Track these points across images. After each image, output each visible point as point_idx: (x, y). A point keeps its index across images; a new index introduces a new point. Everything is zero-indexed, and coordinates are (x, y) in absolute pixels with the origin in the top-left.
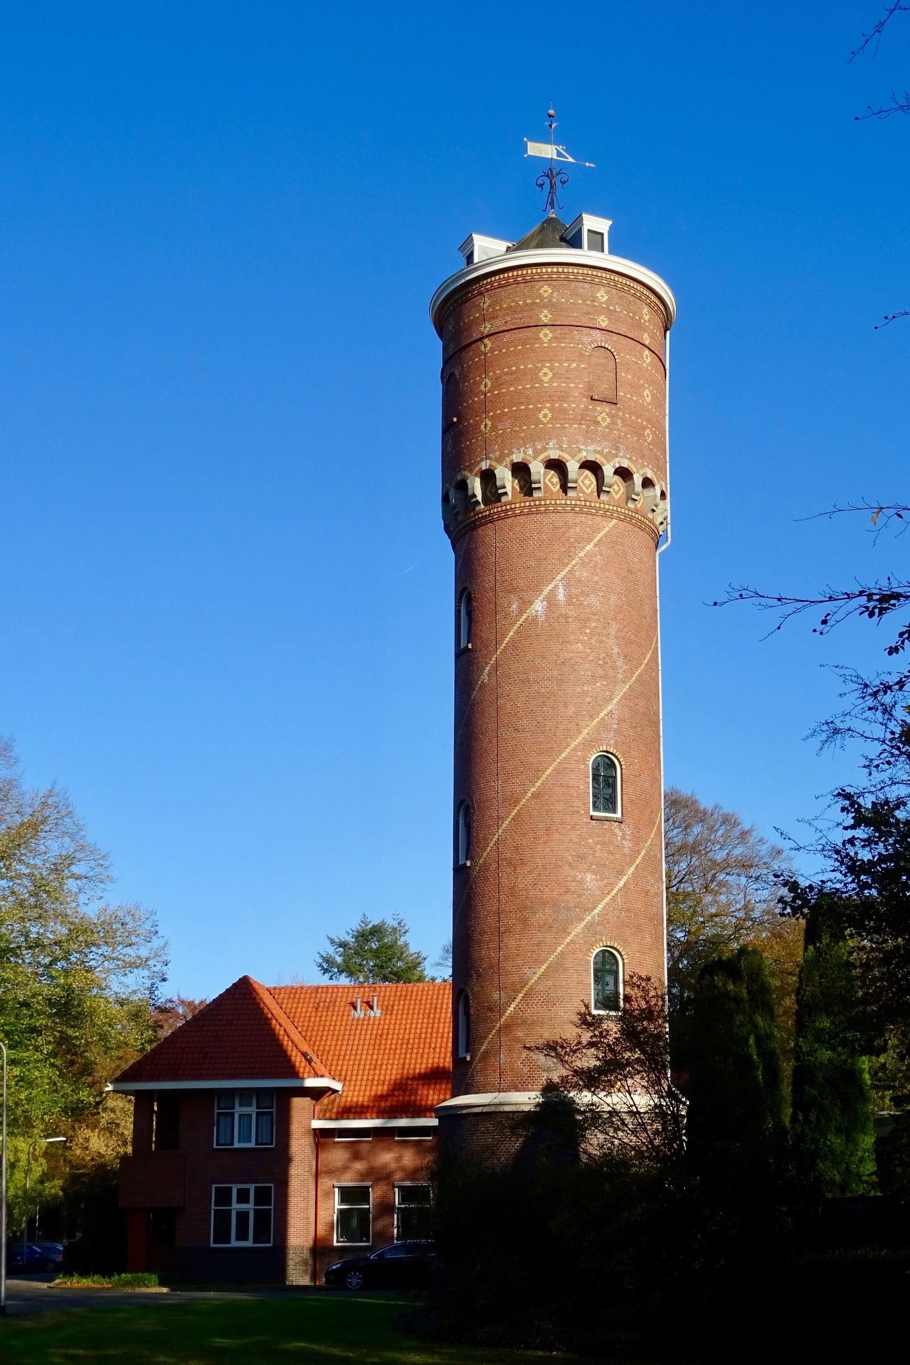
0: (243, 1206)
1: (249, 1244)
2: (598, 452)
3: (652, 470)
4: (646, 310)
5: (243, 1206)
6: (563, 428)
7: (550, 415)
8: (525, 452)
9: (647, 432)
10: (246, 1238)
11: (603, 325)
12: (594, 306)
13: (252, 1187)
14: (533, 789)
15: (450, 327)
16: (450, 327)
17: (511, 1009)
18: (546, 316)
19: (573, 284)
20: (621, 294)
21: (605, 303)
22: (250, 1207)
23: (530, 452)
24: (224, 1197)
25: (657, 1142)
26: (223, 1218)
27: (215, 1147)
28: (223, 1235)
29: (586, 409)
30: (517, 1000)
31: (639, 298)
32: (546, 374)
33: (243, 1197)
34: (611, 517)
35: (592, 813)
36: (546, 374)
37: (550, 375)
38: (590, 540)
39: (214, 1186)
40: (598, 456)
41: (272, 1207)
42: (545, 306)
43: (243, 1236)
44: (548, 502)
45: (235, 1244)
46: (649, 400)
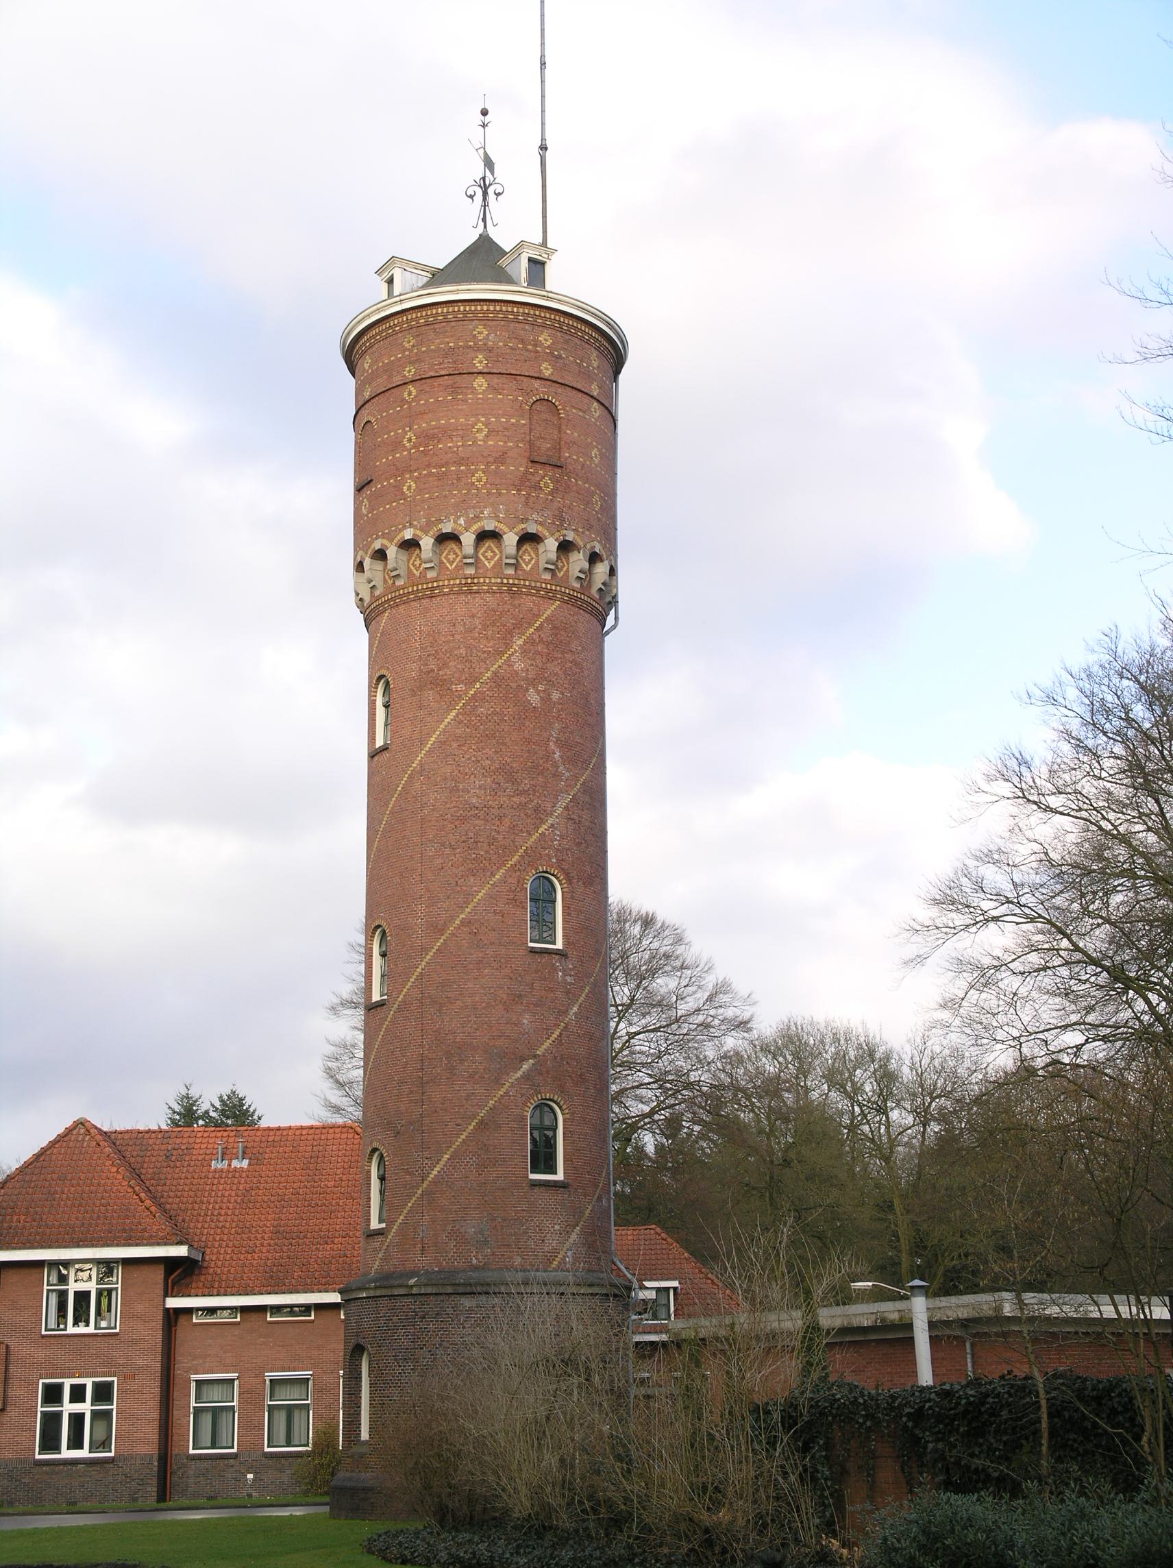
0: (77, 1407)
1: (84, 1453)
2: (541, 524)
3: (600, 542)
4: (595, 354)
5: (77, 1407)
6: (500, 494)
7: (484, 479)
8: (455, 522)
9: (596, 497)
10: (81, 1447)
11: (547, 373)
12: (537, 352)
13: (89, 1382)
14: (462, 916)
15: (366, 366)
16: (366, 366)
17: (435, 1172)
18: (481, 362)
19: (512, 325)
20: (567, 337)
21: (548, 347)
22: (86, 1407)
23: (462, 521)
24: (53, 1395)
25: (990, 1400)
26: (51, 1421)
27: (43, 1332)
28: (50, 1442)
29: (527, 472)
30: (442, 1163)
31: (588, 342)
32: (480, 430)
33: (78, 1394)
34: (553, 599)
35: (533, 1176)
36: (480, 430)
37: (485, 431)
38: (530, 624)
39: (41, 1381)
40: (540, 528)
41: (114, 1407)
42: (479, 350)
43: (76, 1443)
44: (482, 580)
45: (66, 1453)
46: (596, 461)
